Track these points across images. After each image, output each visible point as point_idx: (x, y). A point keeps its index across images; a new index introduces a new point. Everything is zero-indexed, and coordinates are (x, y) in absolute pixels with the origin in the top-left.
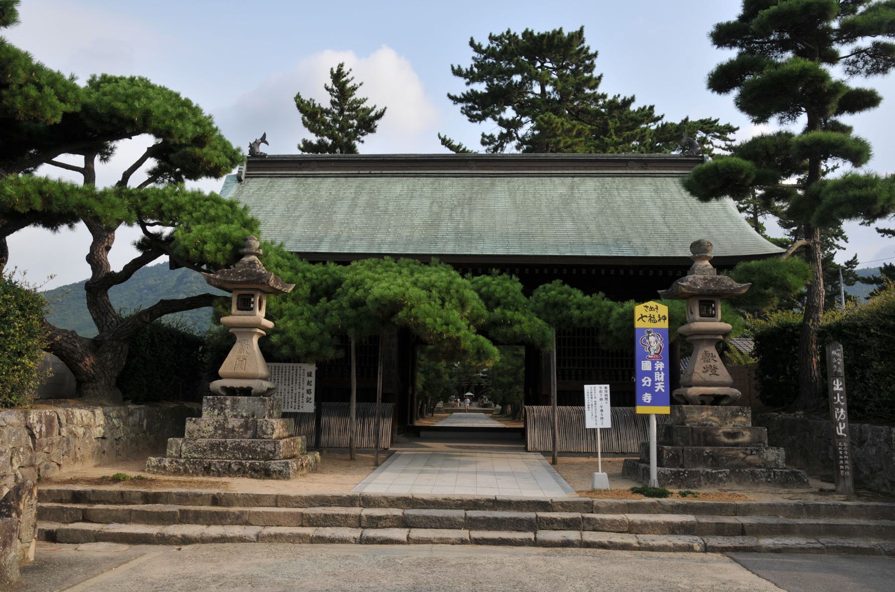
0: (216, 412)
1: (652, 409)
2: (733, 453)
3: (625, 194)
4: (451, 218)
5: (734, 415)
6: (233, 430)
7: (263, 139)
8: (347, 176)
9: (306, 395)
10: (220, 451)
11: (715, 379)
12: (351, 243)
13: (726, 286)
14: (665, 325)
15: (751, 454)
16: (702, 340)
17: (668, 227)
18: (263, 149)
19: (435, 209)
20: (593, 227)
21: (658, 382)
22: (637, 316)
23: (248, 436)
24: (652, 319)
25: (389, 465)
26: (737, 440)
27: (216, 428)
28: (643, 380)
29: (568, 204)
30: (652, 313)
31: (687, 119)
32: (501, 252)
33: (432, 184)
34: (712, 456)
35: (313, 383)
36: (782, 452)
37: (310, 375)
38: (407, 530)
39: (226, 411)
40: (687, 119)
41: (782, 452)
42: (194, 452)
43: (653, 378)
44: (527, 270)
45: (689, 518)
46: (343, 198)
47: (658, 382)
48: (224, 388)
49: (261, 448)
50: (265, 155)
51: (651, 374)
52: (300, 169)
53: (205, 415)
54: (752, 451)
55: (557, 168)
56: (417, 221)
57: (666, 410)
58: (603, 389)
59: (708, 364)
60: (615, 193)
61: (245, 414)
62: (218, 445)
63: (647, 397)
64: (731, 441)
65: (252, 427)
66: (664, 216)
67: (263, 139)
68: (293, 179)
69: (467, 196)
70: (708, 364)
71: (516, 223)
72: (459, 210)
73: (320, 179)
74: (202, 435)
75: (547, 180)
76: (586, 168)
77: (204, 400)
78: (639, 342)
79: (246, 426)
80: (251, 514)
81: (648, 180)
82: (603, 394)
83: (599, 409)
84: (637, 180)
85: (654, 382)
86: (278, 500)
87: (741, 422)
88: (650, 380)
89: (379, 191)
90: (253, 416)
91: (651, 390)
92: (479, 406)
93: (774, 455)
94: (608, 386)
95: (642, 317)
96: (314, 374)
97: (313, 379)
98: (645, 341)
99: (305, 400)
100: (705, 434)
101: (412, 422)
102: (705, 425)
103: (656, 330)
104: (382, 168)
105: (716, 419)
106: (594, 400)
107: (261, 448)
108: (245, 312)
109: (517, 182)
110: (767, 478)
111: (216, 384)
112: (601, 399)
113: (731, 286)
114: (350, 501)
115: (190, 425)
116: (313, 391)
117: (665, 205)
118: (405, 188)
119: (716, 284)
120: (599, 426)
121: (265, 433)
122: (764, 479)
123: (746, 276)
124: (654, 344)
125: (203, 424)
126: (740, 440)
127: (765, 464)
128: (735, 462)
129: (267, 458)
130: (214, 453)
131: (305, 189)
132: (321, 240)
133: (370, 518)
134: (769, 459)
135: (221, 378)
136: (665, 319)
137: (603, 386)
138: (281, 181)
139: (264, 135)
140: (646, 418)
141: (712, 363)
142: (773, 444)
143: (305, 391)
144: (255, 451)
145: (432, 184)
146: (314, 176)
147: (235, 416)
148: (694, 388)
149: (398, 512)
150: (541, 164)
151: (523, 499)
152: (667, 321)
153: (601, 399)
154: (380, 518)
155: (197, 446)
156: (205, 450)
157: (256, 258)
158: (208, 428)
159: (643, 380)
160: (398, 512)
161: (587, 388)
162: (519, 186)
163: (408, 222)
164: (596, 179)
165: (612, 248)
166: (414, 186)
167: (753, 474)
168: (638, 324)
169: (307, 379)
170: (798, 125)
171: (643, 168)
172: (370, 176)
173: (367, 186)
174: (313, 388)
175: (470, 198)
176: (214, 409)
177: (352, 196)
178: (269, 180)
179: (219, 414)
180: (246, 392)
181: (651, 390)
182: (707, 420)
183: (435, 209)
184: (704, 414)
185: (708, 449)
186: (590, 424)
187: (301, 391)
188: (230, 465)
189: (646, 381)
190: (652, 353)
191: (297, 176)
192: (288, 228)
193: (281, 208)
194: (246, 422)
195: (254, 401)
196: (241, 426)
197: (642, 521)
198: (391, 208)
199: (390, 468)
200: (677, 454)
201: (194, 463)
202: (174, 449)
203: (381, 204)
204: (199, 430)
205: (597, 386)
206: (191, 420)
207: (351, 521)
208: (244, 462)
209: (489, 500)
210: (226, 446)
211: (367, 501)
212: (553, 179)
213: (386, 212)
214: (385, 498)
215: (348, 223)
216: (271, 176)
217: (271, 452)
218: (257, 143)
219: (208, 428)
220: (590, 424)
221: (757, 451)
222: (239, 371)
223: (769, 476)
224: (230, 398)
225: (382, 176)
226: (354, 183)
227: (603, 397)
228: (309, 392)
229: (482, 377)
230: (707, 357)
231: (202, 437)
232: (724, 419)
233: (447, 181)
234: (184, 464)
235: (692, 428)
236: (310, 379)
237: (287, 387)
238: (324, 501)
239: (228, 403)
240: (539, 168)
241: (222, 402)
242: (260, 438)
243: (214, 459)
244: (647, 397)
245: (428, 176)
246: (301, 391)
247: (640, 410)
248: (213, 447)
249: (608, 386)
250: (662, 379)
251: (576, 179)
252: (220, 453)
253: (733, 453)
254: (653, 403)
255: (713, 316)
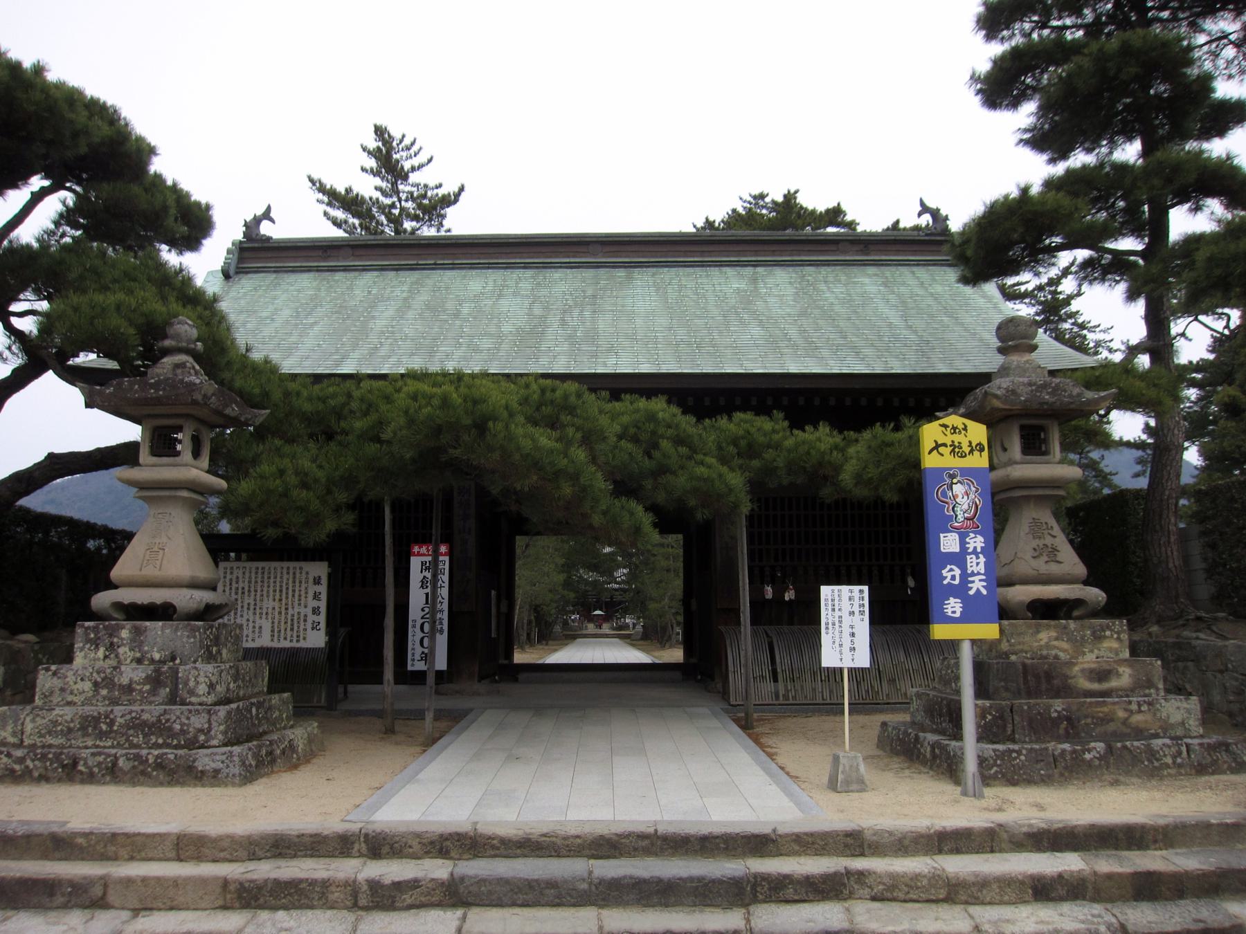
0: (101, 652)
1: (958, 628)
2: (1106, 709)
3: (839, 289)
4: (563, 322)
5: (1098, 638)
6: (129, 689)
7: (267, 215)
8: (397, 269)
9: (311, 618)
10: (101, 731)
11: (1054, 569)
12: (393, 359)
13: (1070, 396)
14: (980, 461)
15: (1140, 711)
16: (1027, 498)
17: (915, 332)
18: (266, 229)
19: (537, 311)
20: (793, 332)
21: (973, 574)
22: (927, 443)
23: (159, 699)
24: (956, 450)
25: (446, 747)
26: (1105, 686)
27: (96, 684)
28: (944, 572)
29: (750, 302)
30: (957, 438)
31: (897, 222)
32: (645, 368)
33: (532, 277)
34: (1068, 719)
35: (324, 597)
36: (1194, 703)
37: (317, 581)
38: (459, 912)
39: (121, 650)
40: (897, 222)
41: (1194, 703)
42: (50, 733)
43: (963, 566)
44: (690, 399)
45: (1071, 863)
46: (389, 299)
47: (973, 574)
48: (118, 606)
49: (182, 725)
50: (269, 239)
51: (959, 559)
52: (325, 259)
53: (79, 660)
54: (1139, 705)
55: (728, 253)
56: (507, 328)
57: (990, 631)
58: (856, 595)
59: (1041, 542)
60: (823, 287)
61: (157, 656)
62: (96, 720)
63: (954, 606)
64: (1095, 686)
65: (163, 678)
66: (905, 318)
67: (267, 215)
68: (312, 275)
69: (589, 292)
70: (1041, 542)
71: (670, 329)
72: (576, 313)
73: (356, 274)
74: (70, 698)
75: (715, 271)
76: (773, 253)
77: (79, 631)
78: (933, 495)
79: (155, 681)
80: (105, 881)
81: (871, 270)
82: (856, 602)
83: (847, 631)
84: (855, 270)
85: (965, 576)
86: (188, 846)
87: (1111, 649)
88: (957, 572)
89: (447, 288)
90: (173, 659)
91: (960, 591)
92: (614, 629)
93: (1181, 711)
94: (866, 588)
95: (937, 446)
96: (324, 581)
97: (323, 589)
98: (944, 494)
99: (309, 626)
100: (1049, 676)
101: (509, 655)
102: (1046, 657)
103: (967, 473)
104: (455, 256)
105: (1065, 645)
106: (837, 613)
107: (182, 725)
108: (165, 460)
109: (667, 274)
110: (1174, 757)
111: (102, 600)
112: (852, 613)
113: (1079, 395)
114: (342, 845)
115: (45, 680)
116: (323, 610)
117: (904, 302)
118: (491, 283)
119: (1052, 394)
120: (847, 663)
121: (192, 692)
122: (1169, 760)
123: (516, 673)
124: (963, 499)
125: (71, 678)
126: (1114, 683)
127: (1166, 728)
128: (1111, 727)
129: (192, 744)
130: (88, 735)
131: (331, 287)
132: (345, 357)
133: (375, 886)
134: (1172, 720)
135: (116, 587)
136: (982, 450)
137: (856, 588)
138: (292, 278)
139: (269, 208)
140: (952, 646)
141: (1049, 541)
142: (1177, 689)
143: (309, 611)
144: (170, 729)
145: (532, 277)
146: (346, 269)
147: (139, 661)
148: (1018, 587)
149: (439, 869)
150: (705, 248)
151: (717, 830)
152: (985, 453)
153: (852, 613)
154: (398, 886)
155: (55, 723)
156: (70, 730)
157: (191, 359)
158: (80, 685)
159: (944, 572)
160: (439, 869)
161: (826, 591)
162: (671, 279)
163: (493, 329)
164: (791, 269)
165: (832, 362)
166: (505, 280)
167: (1152, 754)
168: (930, 461)
169: (313, 589)
170: (1130, 152)
171: (863, 252)
172: (435, 267)
173: (430, 282)
174: (323, 605)
175: (594, 296)
176: (97, 647)
177: (405, 295)
178: (274, 275)
179: (106, 657)
180: (163, 612)
181: (960, 591)
182: (1048, 646)
183: (537, 311)
184: (1044, 636)
185: (1058, 705)
186: (829, 658)
187: (303, 611)
188: (116, 759)
189: (950, 574)
190: (960, 518)
191: (318, 270)
192: (293, 339)
193: (286, 313)
194: (157, 671)
195: (177, 630)
196: (148, 679)
197: (976, 875)
198: (465, 311)
199: (464, 736)
200: (1002, 717)
201: (44, 757)
202: (9, 729)
203: (450, 305)
204: (62, 690)
205: (845, 589)
206: (47, 670)
207: (335, 895)
208: (144, 752)
209: (642, 836)
210: (112, 722)
211: (379, 845)
212: (724, 269)
213: (457, 315)
214: (418, 835)
215: (393, 333)
216: (277, 270)
217: (201, 731)
218: (257, 221)
219: (80, 685)
220: (829, 658)
221: (1150, 704)
222: (150, 572)
223: (1180, 753)
224: (129, 624)
225: (453, 267)
226: (410, 277)
227: (856, 609)
228: (316, 611)
229: (616, 590)
230: (1037, 529)
231: (69, 703)
232: (1079, 646)
233: (557, 274)
234: (21, 760)
235: (1024, 665)
236: (318, 588)
237: (277, 604)
238: (280, 846)
239: (125, 634)
240: (702, 253)
241: (113, 632)
242: (183, 703)
243: (86, 749)
244: (954, 606)
245: (526, 266)
246: (303, 611)
247: (940, 631)
248: (89, 724)
249: (866, 588)
250: (981, 568)
251: (760, 269)
252: (102, 735)
253: (1106, 709)
254: (965, 618)
255: (1046, 453)
